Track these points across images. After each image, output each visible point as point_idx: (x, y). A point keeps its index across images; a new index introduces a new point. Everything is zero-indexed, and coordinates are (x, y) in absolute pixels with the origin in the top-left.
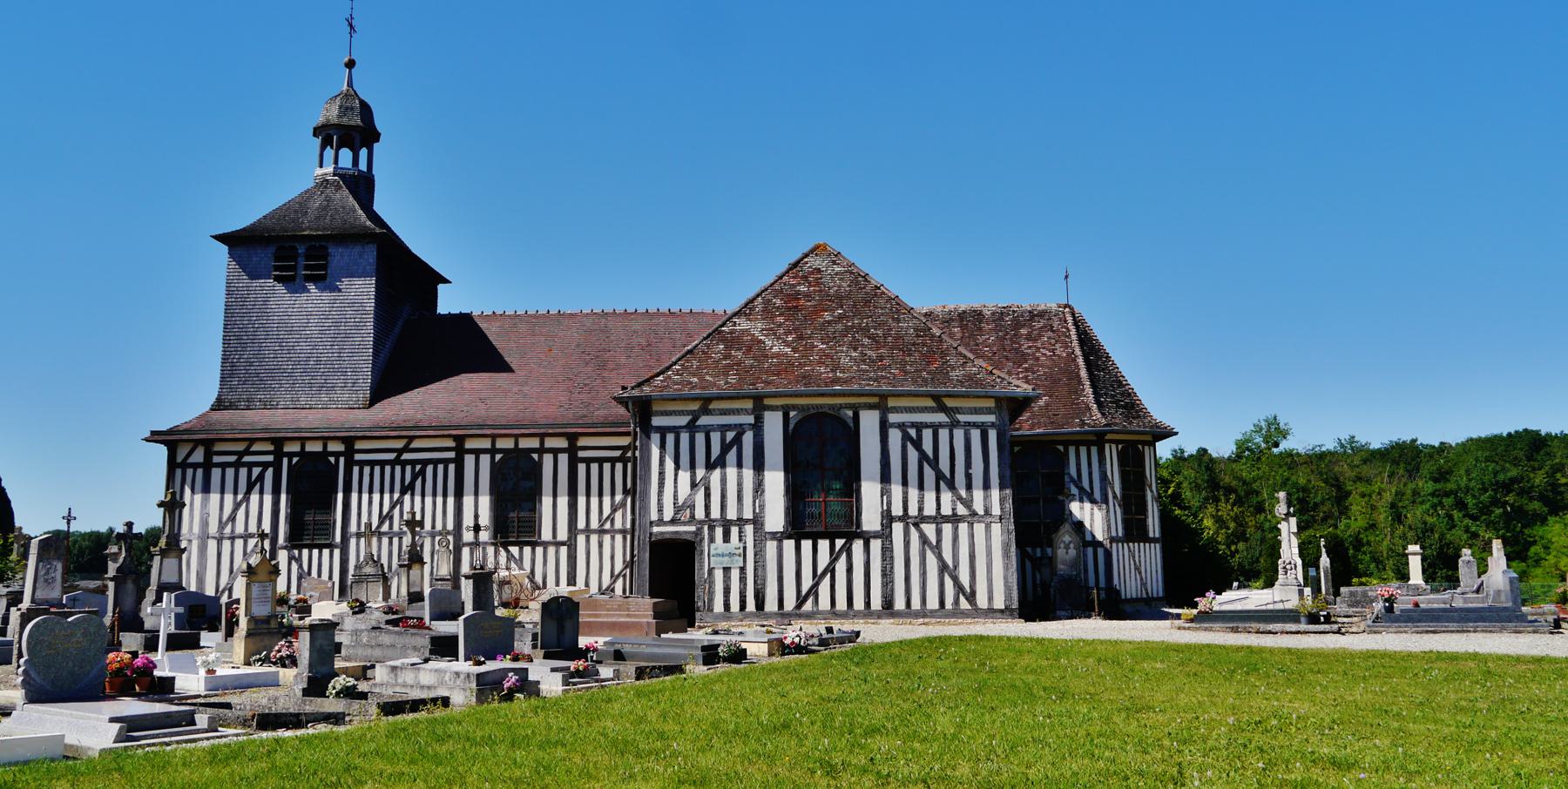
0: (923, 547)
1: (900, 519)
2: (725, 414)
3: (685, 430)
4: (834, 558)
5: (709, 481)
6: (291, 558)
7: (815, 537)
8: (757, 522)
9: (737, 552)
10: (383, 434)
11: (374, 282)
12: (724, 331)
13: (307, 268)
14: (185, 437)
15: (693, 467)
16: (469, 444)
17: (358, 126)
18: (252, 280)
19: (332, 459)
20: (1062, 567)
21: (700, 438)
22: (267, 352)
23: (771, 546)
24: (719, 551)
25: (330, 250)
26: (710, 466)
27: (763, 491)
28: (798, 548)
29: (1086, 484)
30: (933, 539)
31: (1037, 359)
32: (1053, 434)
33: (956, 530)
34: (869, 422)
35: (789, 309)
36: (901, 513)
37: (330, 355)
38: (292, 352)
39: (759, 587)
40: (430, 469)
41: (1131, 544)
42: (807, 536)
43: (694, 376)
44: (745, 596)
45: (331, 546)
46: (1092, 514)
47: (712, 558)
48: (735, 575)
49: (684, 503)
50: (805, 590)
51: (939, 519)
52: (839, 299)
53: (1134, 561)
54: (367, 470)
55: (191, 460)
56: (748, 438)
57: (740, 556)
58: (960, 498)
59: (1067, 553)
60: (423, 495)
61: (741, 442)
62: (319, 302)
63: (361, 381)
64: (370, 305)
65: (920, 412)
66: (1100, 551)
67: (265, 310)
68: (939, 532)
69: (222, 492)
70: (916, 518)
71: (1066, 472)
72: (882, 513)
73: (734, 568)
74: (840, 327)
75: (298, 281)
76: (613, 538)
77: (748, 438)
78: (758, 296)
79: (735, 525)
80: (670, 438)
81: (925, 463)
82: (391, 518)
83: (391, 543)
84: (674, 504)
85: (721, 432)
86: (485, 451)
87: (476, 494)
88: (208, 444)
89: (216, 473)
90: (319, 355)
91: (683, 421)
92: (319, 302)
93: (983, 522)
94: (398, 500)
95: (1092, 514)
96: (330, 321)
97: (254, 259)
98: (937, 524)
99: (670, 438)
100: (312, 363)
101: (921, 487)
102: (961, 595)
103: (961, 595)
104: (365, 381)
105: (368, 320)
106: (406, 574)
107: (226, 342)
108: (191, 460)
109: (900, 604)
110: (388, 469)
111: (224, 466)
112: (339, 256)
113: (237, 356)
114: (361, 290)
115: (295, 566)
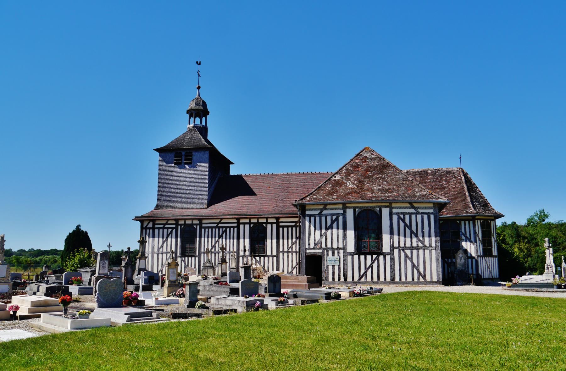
0: (406, 258)
1: (397, 248)
2: (332, 210)
3: (318, 216)
4: (373, 262)
6: (182, 260)
7: (365, 254)
8: (344, 249)
9: (337, 259)
10: (212, 217)
11: (208, 164)
12: (331, 180)
13: (185, 160)
14: (146, 219)
15: (321, 229)
16: (242, 221)
17: (202, 110)
19: (195, 226)
20: (459, 266)
21: (323, 218)
23: (349, 258)
24: (331, 259)
25: (193, 153)
26: (327, 229)
27: (346, 238)
28: (359, 258)
29: (468, 235)
31: (449, 188)
32: (456, 216)
33: (418, 252)
34: (385, 212)
35: (355, 171)
36: (397, 246)
37: (194, 190)
39: (345, 272)
40: (228, 230)
41: (486, 258)
42: (362, 254)
43: (321, 196)
45: (195, 256)
46: (470, 247)
47: (328, 262)
48: (336, 268)
50: (362, 273)
51: (412, 248)
52: (374, 167)
53: (487, 264)
54: (207, 230)
55: (148, 227)
56: (341, 218)
58: (420, 240)
59: (461, 261)
60: (226, 239)
61: (338, 220)
62: (190, 171)
63: (204, 199)
64: (207, 172)
66: (474, 260)
68: (412, 253)
69: (159, 238)
70: (403, 247)
71: (460, 231)
72: (390, 246)
73: (336, 265)
74: (374, 177)
75: (182, 164)
76: (292, 254)
77: (341, 218)
78: (344, 167)
79: (336, 250)
80: (313, 218)
82: (215, 247)
83: (215, 256)
84: (314, 242)
85: (331, 216)
86: (247, 223)
87: (244, 238)
88: (154, 221)
89: (156, 231)
91: (317, 212)
92: (190, 171)
93: (429, 249)
95: (470, 247)
97: (168, 157)
98: (411, 250)
99: (313, 218)
100: (187, 193)
101: (405, 236)
102: (420, 276)
103: (420, 276)
106: (221, 266)
109: (397, 279)
110: (214, 230)
111: (159, 228)
112: (196, 155)
113: (163, 191)
114: (204, 167)
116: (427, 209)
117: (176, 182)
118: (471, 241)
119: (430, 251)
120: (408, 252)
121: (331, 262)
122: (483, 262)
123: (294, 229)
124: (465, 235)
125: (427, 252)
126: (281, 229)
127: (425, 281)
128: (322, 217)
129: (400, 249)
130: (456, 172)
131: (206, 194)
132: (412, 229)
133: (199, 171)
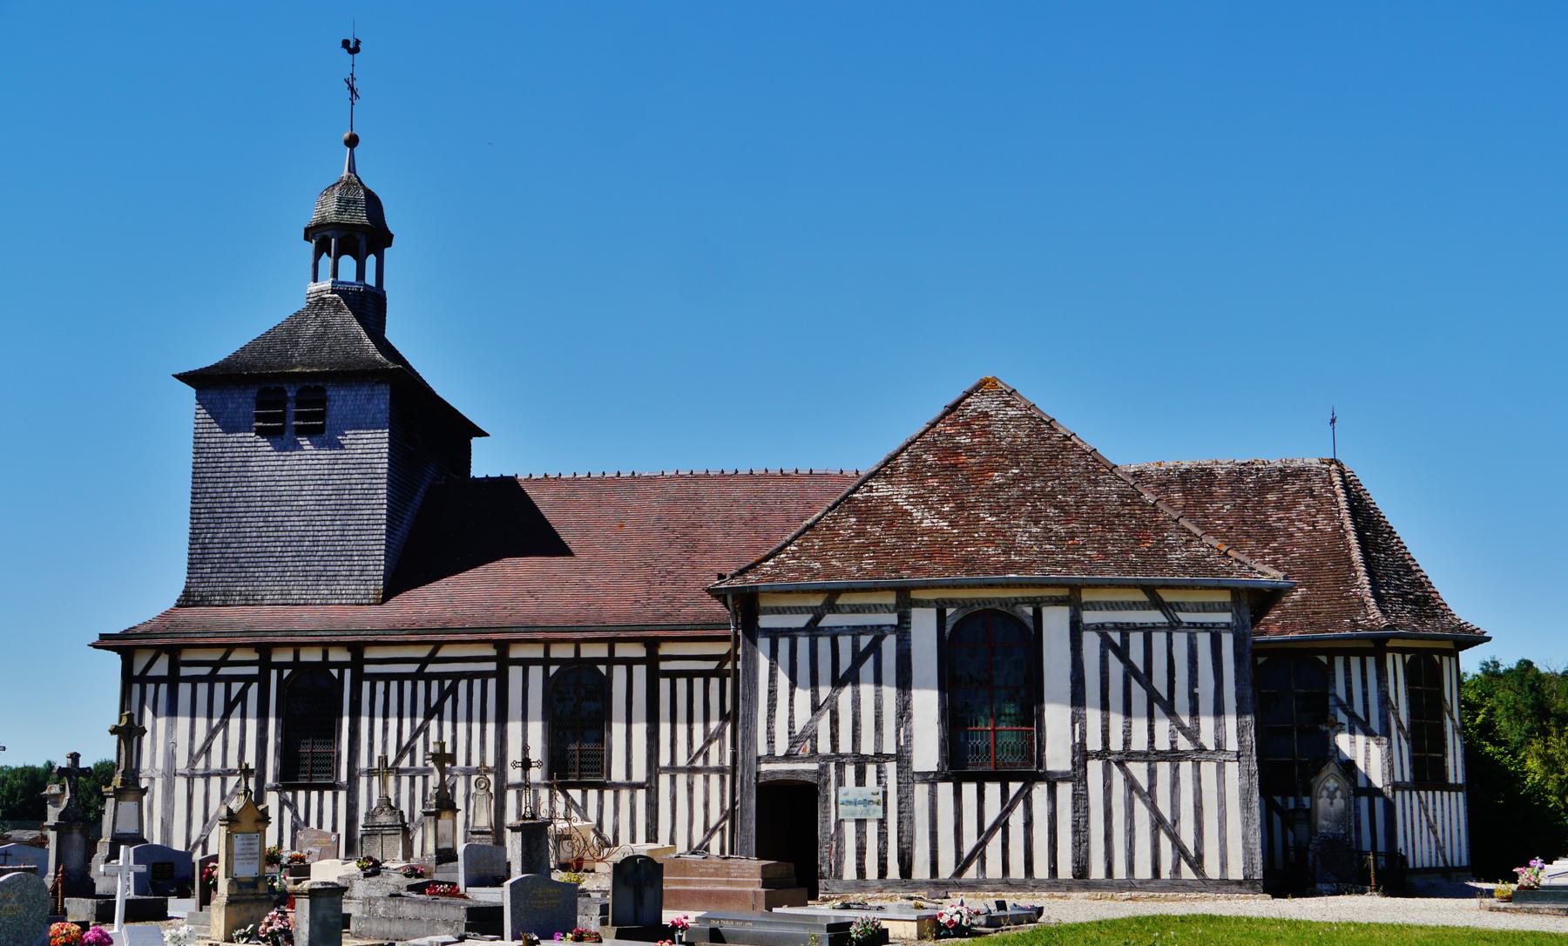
0: (1130, 794)
3: (804, 634)
4: (1007, 807)
5: (837, 703)
6: (283, 803)
7: (981, 779)
8: (902, 758)
9: (875, 798)
11: (386, 435)
12: (856, 499)
13: (299, 416)
14: (144, 642)
15: (814, 683)
17: (363, 225)
18: (228, 433)
19: (335, 672)
20: (1325, 823)
21: (824, 644)
22: (248, 530)
23: (921, 792)
24: (850, 798)
25: (328, 393)
27: (910, 717)
29: (1358, 708)
30: (1143, 783)
31: (1291, 535)
32: (1313, 640)
34: (1055, 622)
35: (945, 468)
36: (1099, 747)
37: (330, 533)
38: (281, 529)
39: (905, 846)
41: (1422, 793)
43: (816, 559)
44: (886, 859)
45: (335, 788)
46: (1367, 751)
47: (840, 807)
48: (872, 830)
49: (802, 732)
51: (1151, 756)
52: (1014, 454)
53: (1427, 816)
54: (380, 686)
55: (152, 672)
56: (889, 645)
57: (878, 803)
58: (1182, 728)
59: (1331, 803)
60: (454, 721)
61: (880, 649)
62: (316, 462)
63: (372, 568)
64: (383, 467)
65: (1126, 609)
66: (1379, 802)
67: (244, 474)
68: (1152, 774)
69: (193, 715)
70: (1120, 753)
72: (1073, 747)
73: (871, 820)
74: (1015, 492)
75: (287, 434)
77: (889, 645)
78: (903, 449)
79: (872, 762)
80: (784, 644)
81: (1133, 680)
82: (413, 751)
83: (412, 784)
84: (790, 733)
85: (853, 636)
86: (535, 661)
87: (525, 718)
88: (173, 651)
89: (184, 690)
90: (316, 533)
91: (801, 620)
92: (316, 462)
93: (1214, 760)
94: (421, 726)
95: (1367, 751)
96: (330, 487)
97: (230, 406)
98: (1150, 762)
99: (784, 644)
100: (307, 543)
101: (1127, 712)
104: (377, 568)
105: (380, 486)
106: (433, 825)
107: (195, 516)
108: (151, 673)
109: (1097, 871)
110: (408, 685)
111: (194, 680)
112: (340, 400)
113: (209, 536)
114: (370, 446)
115: (287, 813)
116: (1210, 612)
117: (260, 504)
118: (1371, 730)
119: (1221, 768)
120: (1139, 770)
121: (852, 807)
122: (1411, 807)
123: (715, 683)
124: (1347, 707)
125: (1209, 769)
126: (665, 684)
127: (1201, 877)
128: (820, 640)
129: (1108, 760)
130: (1316, 475)
131: (378, 547)
132: (1155, 684)
133: (350, 461)
